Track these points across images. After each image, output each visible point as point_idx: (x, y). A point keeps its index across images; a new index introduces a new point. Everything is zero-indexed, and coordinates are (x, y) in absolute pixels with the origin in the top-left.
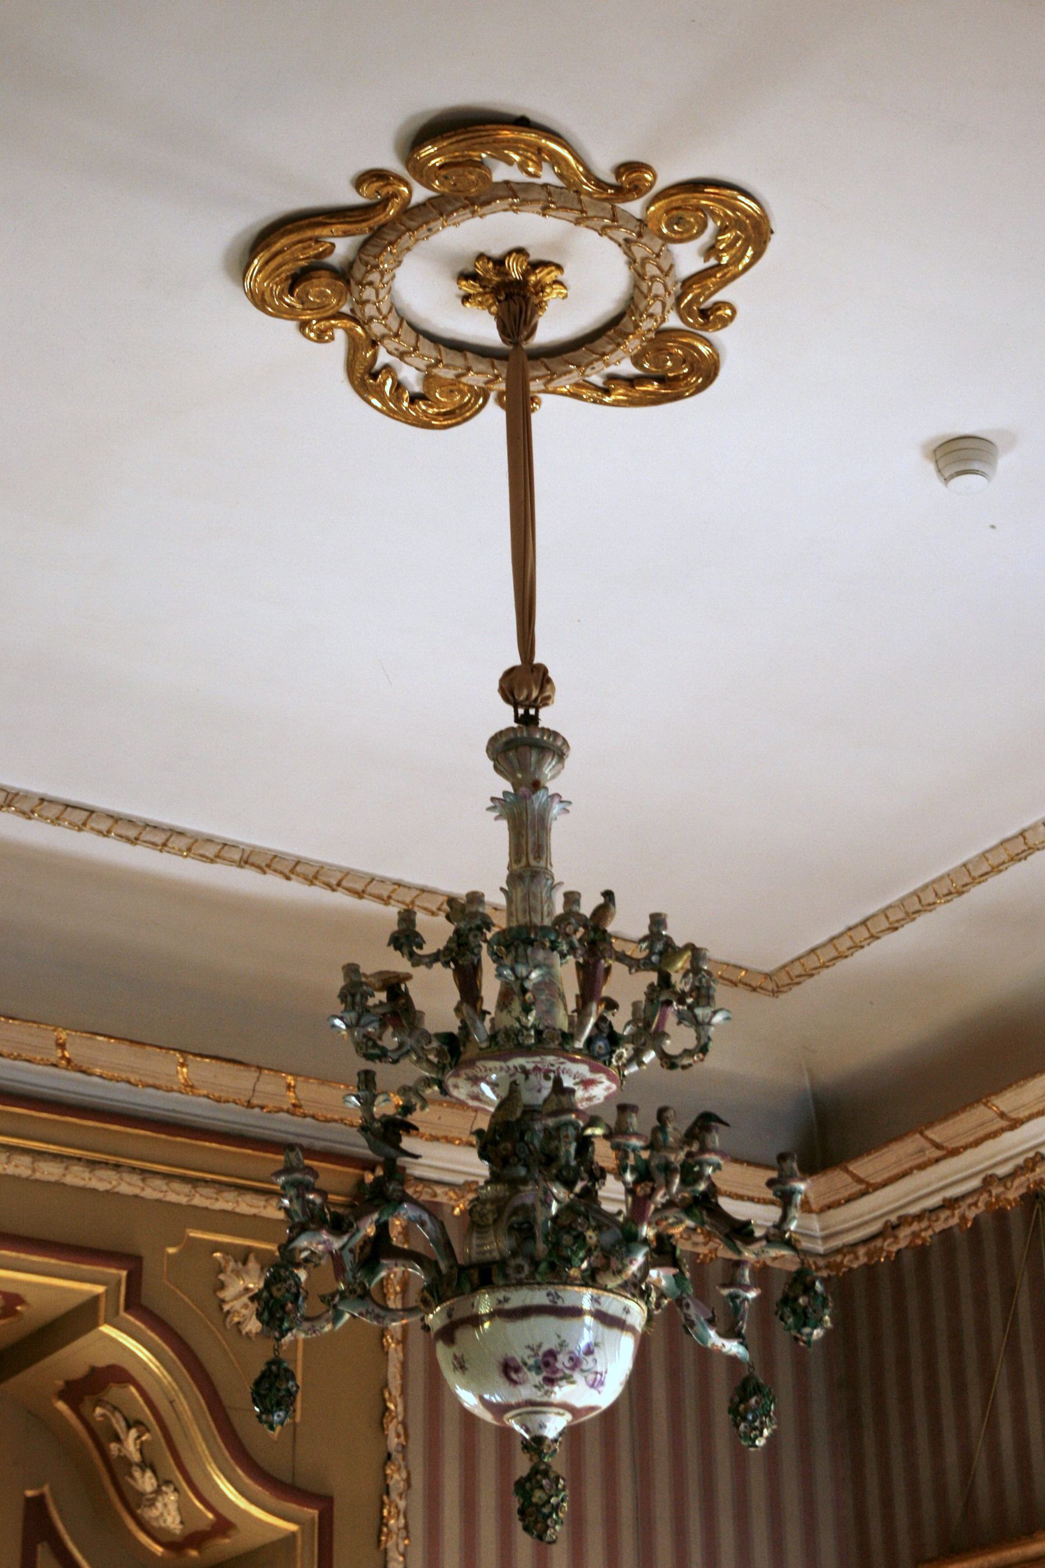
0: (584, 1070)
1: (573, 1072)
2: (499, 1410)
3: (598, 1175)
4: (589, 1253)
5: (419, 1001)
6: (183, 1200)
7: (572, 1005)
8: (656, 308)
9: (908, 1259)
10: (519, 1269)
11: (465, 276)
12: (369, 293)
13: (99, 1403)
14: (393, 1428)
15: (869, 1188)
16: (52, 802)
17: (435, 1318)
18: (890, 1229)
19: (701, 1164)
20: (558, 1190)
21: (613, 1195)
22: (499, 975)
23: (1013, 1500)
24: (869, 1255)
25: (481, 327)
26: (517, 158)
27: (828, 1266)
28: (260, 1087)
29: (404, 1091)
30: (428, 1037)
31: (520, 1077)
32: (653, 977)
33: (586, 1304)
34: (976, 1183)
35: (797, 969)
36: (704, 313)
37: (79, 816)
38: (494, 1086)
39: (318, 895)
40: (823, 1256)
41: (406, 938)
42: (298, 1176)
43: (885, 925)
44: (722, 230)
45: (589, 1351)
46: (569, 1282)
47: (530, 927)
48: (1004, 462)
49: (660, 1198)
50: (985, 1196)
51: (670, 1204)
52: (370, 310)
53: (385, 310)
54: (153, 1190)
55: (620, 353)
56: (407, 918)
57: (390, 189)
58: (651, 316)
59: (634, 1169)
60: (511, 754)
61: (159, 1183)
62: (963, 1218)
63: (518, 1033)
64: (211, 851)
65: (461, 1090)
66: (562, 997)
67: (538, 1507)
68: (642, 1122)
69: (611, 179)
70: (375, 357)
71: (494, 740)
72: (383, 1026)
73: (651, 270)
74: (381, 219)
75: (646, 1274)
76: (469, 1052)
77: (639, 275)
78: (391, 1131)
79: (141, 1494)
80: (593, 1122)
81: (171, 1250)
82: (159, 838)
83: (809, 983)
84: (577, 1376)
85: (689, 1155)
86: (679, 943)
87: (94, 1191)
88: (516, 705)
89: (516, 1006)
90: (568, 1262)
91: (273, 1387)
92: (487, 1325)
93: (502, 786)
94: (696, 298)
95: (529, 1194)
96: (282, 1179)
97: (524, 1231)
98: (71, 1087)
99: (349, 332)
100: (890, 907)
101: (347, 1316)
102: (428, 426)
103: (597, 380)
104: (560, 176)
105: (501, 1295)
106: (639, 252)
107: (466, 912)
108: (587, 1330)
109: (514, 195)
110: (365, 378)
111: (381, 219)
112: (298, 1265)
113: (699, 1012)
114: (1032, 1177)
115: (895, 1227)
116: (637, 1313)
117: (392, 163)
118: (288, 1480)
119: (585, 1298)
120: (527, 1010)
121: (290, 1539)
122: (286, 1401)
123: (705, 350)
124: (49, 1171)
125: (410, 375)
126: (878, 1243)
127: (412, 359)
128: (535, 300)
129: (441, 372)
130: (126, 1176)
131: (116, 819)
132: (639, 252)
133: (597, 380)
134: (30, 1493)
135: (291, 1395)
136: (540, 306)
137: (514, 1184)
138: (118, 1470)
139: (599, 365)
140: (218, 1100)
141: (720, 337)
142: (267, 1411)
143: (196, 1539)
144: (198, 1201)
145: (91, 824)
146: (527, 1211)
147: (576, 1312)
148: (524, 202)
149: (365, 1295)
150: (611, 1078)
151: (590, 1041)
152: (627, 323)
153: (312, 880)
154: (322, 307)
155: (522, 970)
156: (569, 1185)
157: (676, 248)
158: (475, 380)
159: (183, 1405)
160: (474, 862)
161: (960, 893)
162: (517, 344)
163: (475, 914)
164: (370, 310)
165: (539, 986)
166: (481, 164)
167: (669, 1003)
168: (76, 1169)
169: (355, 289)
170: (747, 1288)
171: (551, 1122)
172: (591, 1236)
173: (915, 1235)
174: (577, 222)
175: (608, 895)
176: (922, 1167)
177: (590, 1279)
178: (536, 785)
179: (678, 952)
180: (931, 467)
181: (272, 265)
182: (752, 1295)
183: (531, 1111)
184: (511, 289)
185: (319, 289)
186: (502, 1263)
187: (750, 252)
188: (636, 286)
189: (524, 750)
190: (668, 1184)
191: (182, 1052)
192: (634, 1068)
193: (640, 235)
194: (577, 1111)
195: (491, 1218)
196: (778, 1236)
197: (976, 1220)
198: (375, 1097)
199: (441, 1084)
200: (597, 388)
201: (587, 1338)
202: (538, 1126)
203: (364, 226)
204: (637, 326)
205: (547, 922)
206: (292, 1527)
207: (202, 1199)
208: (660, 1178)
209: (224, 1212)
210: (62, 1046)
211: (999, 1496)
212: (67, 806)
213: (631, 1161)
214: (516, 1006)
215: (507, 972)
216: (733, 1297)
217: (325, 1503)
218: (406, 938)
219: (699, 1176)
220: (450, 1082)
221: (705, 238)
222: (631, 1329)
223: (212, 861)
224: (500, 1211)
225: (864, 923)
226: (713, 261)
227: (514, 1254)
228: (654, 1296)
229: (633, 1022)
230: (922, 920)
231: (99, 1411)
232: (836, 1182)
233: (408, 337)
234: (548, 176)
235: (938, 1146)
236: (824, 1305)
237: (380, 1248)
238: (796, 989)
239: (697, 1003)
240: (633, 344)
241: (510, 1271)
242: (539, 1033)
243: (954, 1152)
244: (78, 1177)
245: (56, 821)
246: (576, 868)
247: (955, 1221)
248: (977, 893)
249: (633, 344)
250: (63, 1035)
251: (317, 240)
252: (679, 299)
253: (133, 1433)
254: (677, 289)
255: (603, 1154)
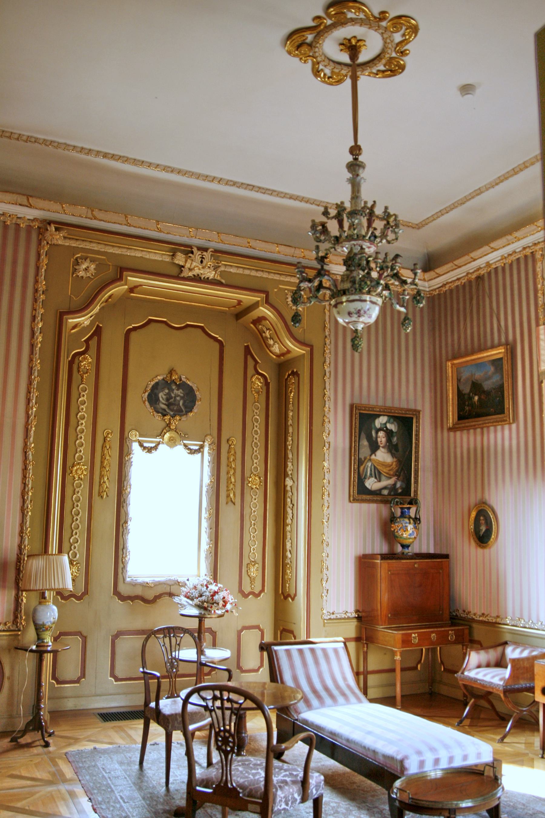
0: (368, 244)
1: (365, 245)
2: (348, 323)
3: (371, 269)
4: (368, 286)
5: (329, 229)
6: (278, 279)
7: (366, 229)
8: (389, 51)
9: (448, 292)
10: (352, 291)
11: (341, 44)
12: (317, 50)
13: (260, 325)
14: (327, 330)
15: (439, 276)
16: (244, 184)
17: (333, 302)
18: (444, 285)
19: (395, 266)
20: (361, 272)
21: (374, 275)
22: (348, 221)
23: (469, 347)
24: (439, 291)
25: (345, 58)
26: (353, 11)
27: (429, 294)
28: (296, 252)
29: (326, 250)
30: (331, 237)
31: (353, 246)
32: (385, 222)
33: (368, 299)
34: (465, 274)
35: (424, 223)
36: (402, 52)
37: (251, 187)
38: (347, 248)
39: (308, 206)
40: (429, 291)
41: (326, 213)
42: (300, 269)
43: (445, 211)
44: (406, 29)
45: (368, 310)
46: (363, 294)
47: (356, 210)
48: (478, 91)
49: (385, 274)
50: (467, 277)
51: (388, 276)
52: (317, 54)
53: (321, 54)
54: (271, 276)
55: (380, 64)
56: (326, 208)
57: (321, 21)
58: (388, 53)
59: (379, 267)
60: (352, 167)
61: (272, 275)
62: (461, 283)
63: (352, 235)
64: (282, 195)
65: (339, 250)
66: (363, 227)
67: (356, 345)
68: (381, 256)
69: (377, 16)
70: (319, 67)
71: (348, 164)
72: (321, 234)
73: (388, 41)
74: (319, 29)
75: (382, 292)
76: (341, 240)
77: (385, 42)
78: (322, 260)
79: (270, 345)
80: (370, 257)
81: (276, 290)
82: (270, 192)
83: (426, 227)
84: (365, 315)
85: (393, 264)
86: (392, 213)
87: (257, 277)
88: (353, 155)
89: (352, 229)
90: (363, 288)
91: (296, 318)
92: (344, 304)
93: (350, 175)
94: (399, 49)
95: (355, 274)
96: (297, 270)
97: (354, 282)
98: (252, 253)
99: (312, 60)
100: (447, 207)
101: (313, 302)
102: (332, 85)
103: (374, 71)
104: (365, 16)
105: (348, 297)
106: (385, 36)
107: (340, 208)
108: (368, 305)
109: (353, 21)
110: (316, 73)
111: (319, 29)
112: (301, 291)
113: (396, 230)
114: (478, 273)
115: (445, 285)
116: (380, 301)
117: (321, 14)
118: (303, 341)
119: (368, 297)
120: (354, 229)
121: (304, 355)
122: (299, 321)
123: (402, 62)
124: (247, 272)
125: (328, 72)
126: (441, 288)
127: (328, 67)
128: (358, 50)
129: (336, 71)
130: (265, 273)
131: (260, 188)
132: (385, 36)
133: (374, 71)
134: (245, 344)
135: (300, 320)
136: (360, 52)
137: (351, 271)
138: (265, 339)
139: (375, 67)
140: (286, 255)
141: (405, 58)
142: (295, 323)
143: (283, 355)
144: (281, 279)
145: (254, 189)
146: (354, 277)
147: (365, 301)
148: (356, 23)
149: (317, 297)
150: (375, 246)
151: (370, 238)
152: (382, 55)
153: (307, 202)
154: (305, 54)
155: (353, 220)
156: (364, 271)
157: (395, 35)
158: (344, 72)
159: (279, 325)
160: (343, 195)
161: (464, 204)
162: (354, 62)
163: (342, 207)
164: (317, 54)
165: (358, 224)
166: (344, 13)
167: (389, 228)
168: (253, 271)
169: (313, 48)
170: (406, 296)
171: (359, 256)
172: (369, 283)
173: (450, 286)
174: (369, 28)
175: (375, 202)
176: (452, 270)
177: (369, 293)
178: (358, 175)
179: (392, 216)
180: (459, 93)
181: (292, 43)
182: (407, 297)
183: (355, 254)
184: (352, 47)
185: (304, 49)
186: (348, 290)
187: (414, 35)
188: (384, 46)
189: (355, 167)
190: (387, 271)
191: (277, 244)
192: (380, 244)
193: (385, 31)
194: (366, 254)
195: (346, 279)
196: (413, 283)
197: (464, 283)
198: (319, 251)
199: (334, 248)
200: (374, 73)
201: (368, 307)
202: (357, 258)
203: (315, 31)
204: (384, 56)
205: (360, 209)
206: (304, 352)
207: (282, 278)
208: (385, 269)
209: (287, 281)
210: (249, 243)
211: (466, 346)
212: (248, 185)
213: (379, 265)
214: (352, 229)
215: (350, 221)
216: (403, 298)
217: (311, 347)
218: (326, 213)
219: (395, 269)
220: (337, 247)
221: (402, 32)
222: (378, 305)
223: (283, 198)
224: (348, 277)
225: (440, 211)
226: (404, 38)
227: (351, 287)
228: (384, 297)
229: (381, 233)
230: (454, 211)
231: (260, 326)
232: (431, 274)
233: (327, 61)
234: (362, 16)
235: (456, 265)
236: (423, 299)
237: (320, 286)
238: (423, 228)
239: (396, 228)
240: (384, 61)
241: (350, 291)
242: (357, 235)
243: (460, 267)
244: (253, 273)
245: (246, 189)
246: (367, 195)
247: (459, 283)
248: (468, 204)
249: (384, 61)
250: (249, 240)
251: (303, 36)
252: (395, 49)
253: (268, 331)
254: (395, 46)
255: (373, 265)
